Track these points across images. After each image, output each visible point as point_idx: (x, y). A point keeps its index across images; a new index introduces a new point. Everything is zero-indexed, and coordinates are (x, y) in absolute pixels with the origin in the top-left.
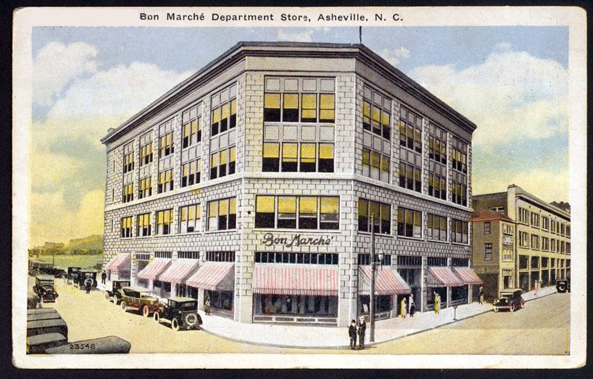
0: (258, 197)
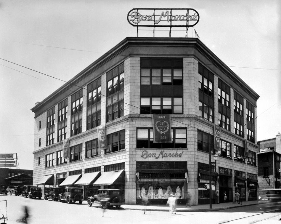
0: (182, 112)
